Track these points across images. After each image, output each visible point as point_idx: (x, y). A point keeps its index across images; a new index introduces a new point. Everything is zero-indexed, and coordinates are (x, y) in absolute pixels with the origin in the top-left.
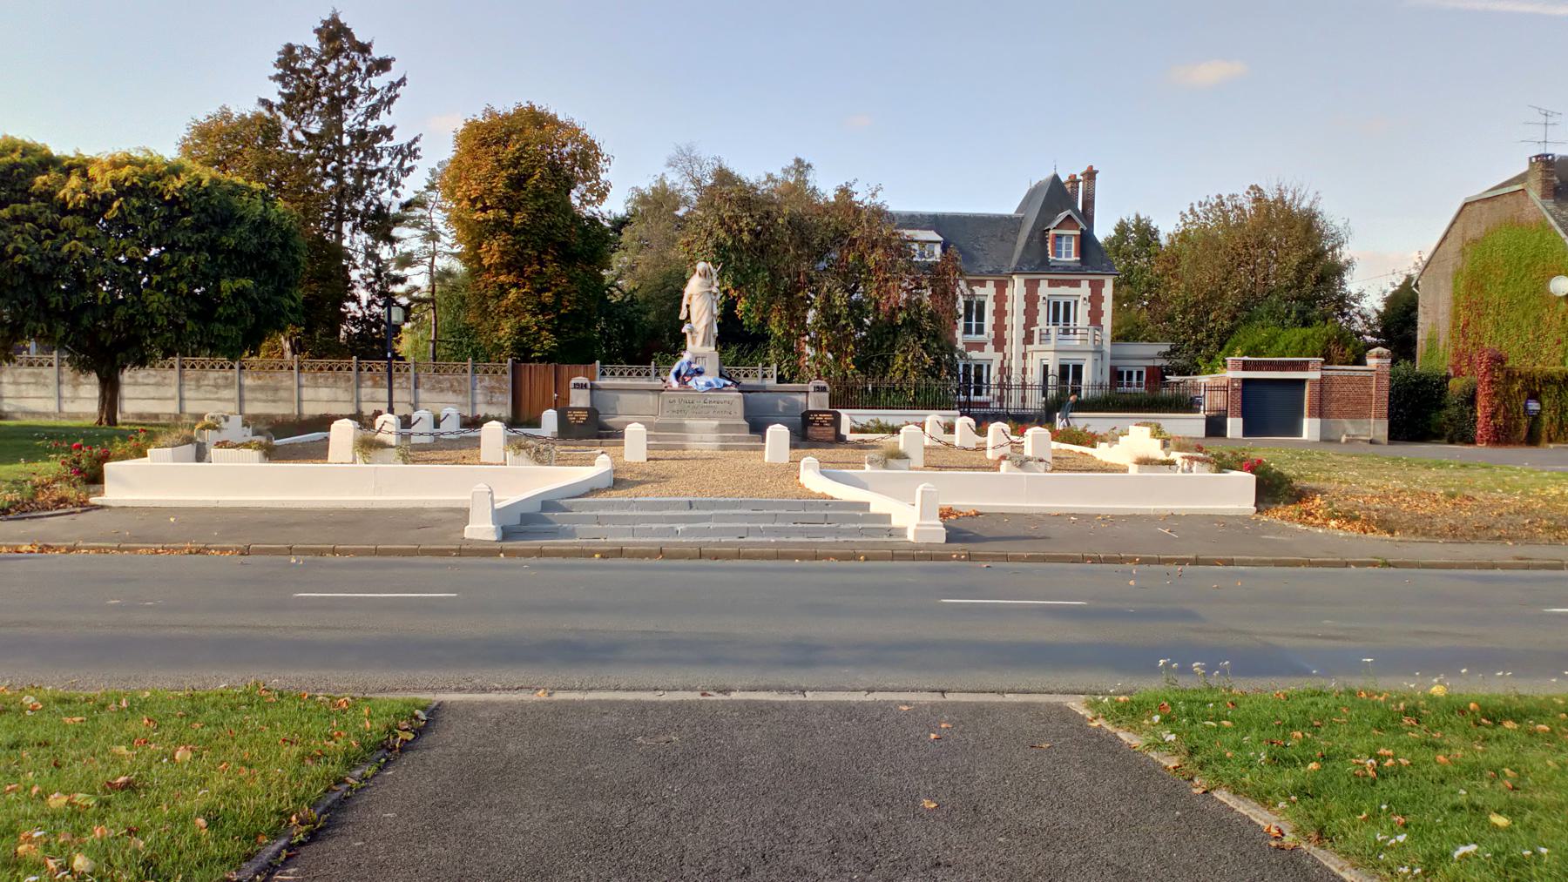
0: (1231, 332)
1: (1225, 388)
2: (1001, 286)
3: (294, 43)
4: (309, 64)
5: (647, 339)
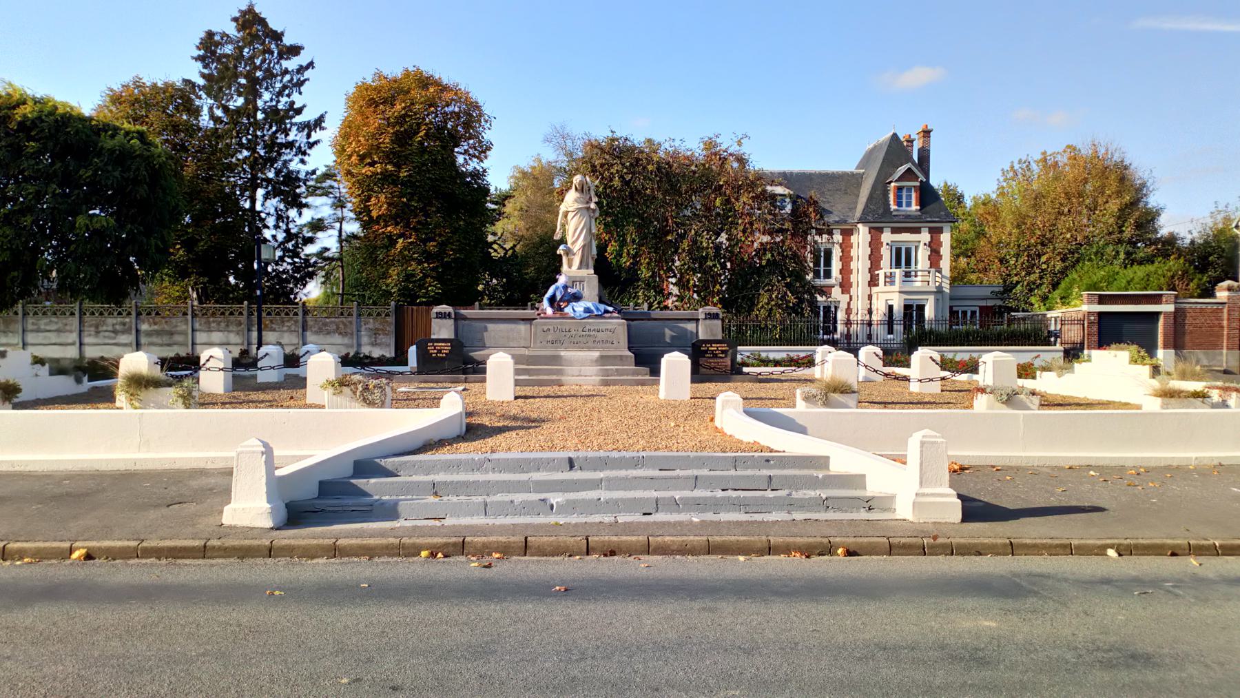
0: (1064, 272)
1: (1081, 322)
2: (847, 233)
3: (214, 30)
4: (228, 49)
5: (526, 278)
